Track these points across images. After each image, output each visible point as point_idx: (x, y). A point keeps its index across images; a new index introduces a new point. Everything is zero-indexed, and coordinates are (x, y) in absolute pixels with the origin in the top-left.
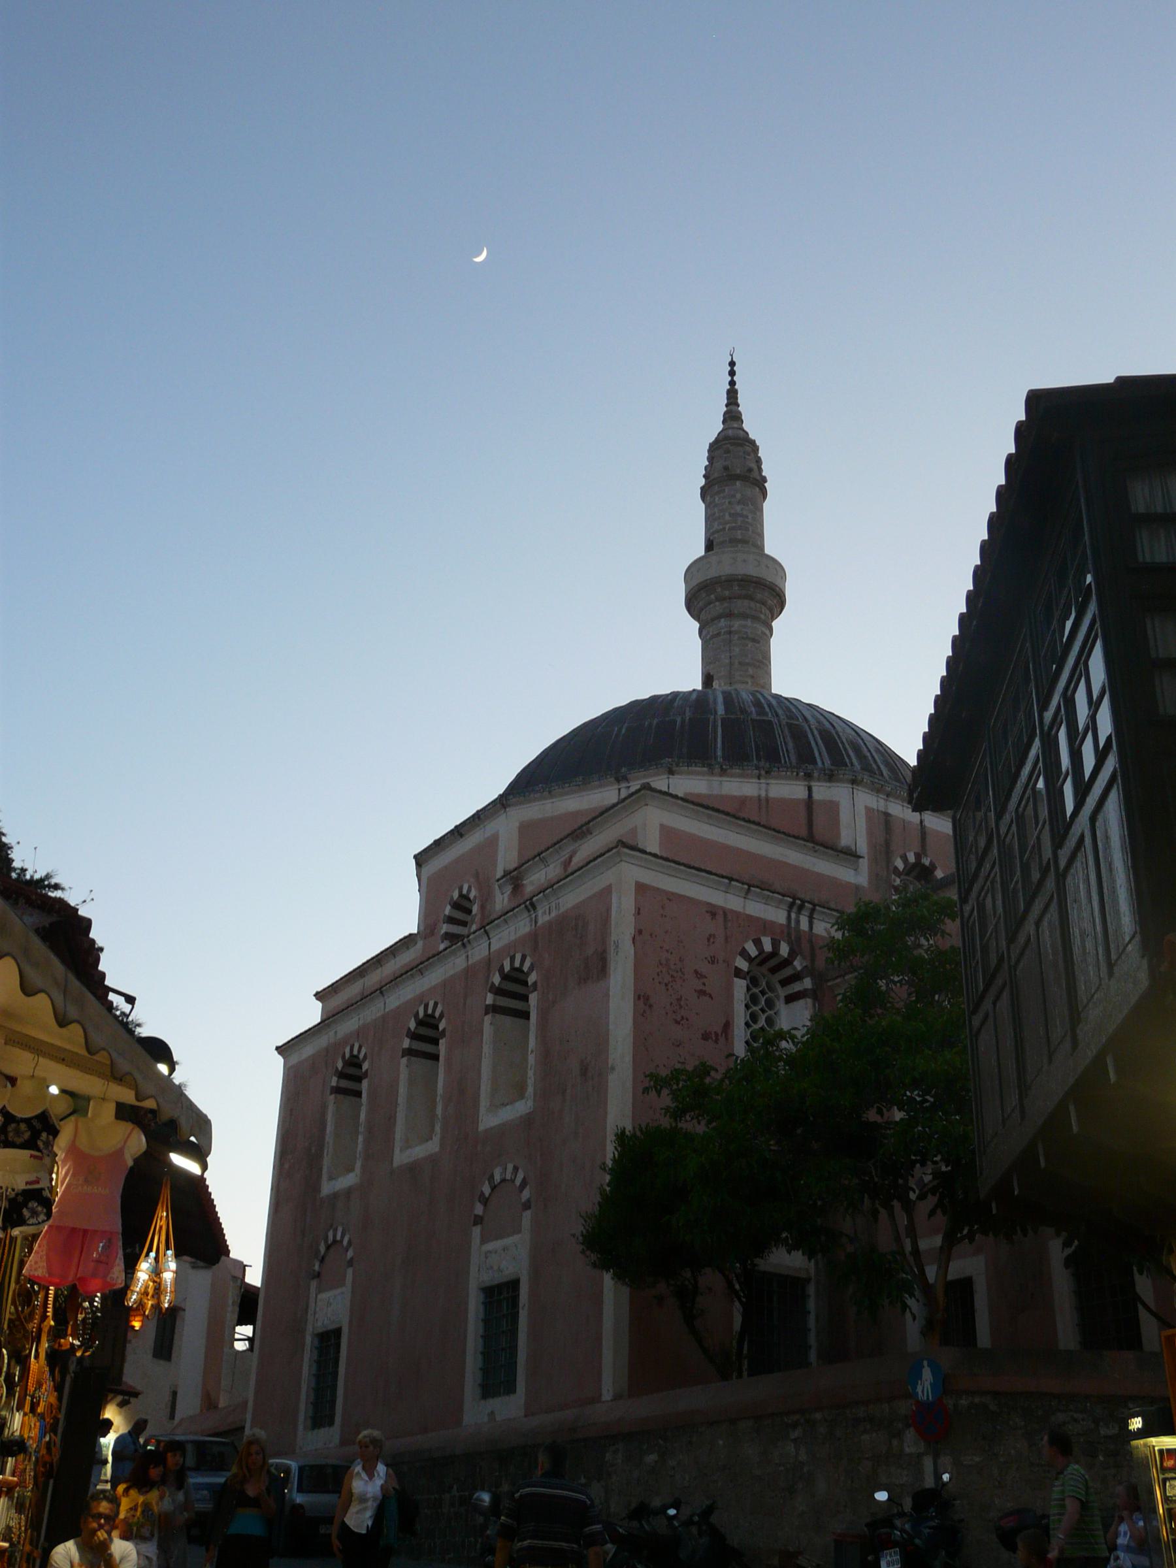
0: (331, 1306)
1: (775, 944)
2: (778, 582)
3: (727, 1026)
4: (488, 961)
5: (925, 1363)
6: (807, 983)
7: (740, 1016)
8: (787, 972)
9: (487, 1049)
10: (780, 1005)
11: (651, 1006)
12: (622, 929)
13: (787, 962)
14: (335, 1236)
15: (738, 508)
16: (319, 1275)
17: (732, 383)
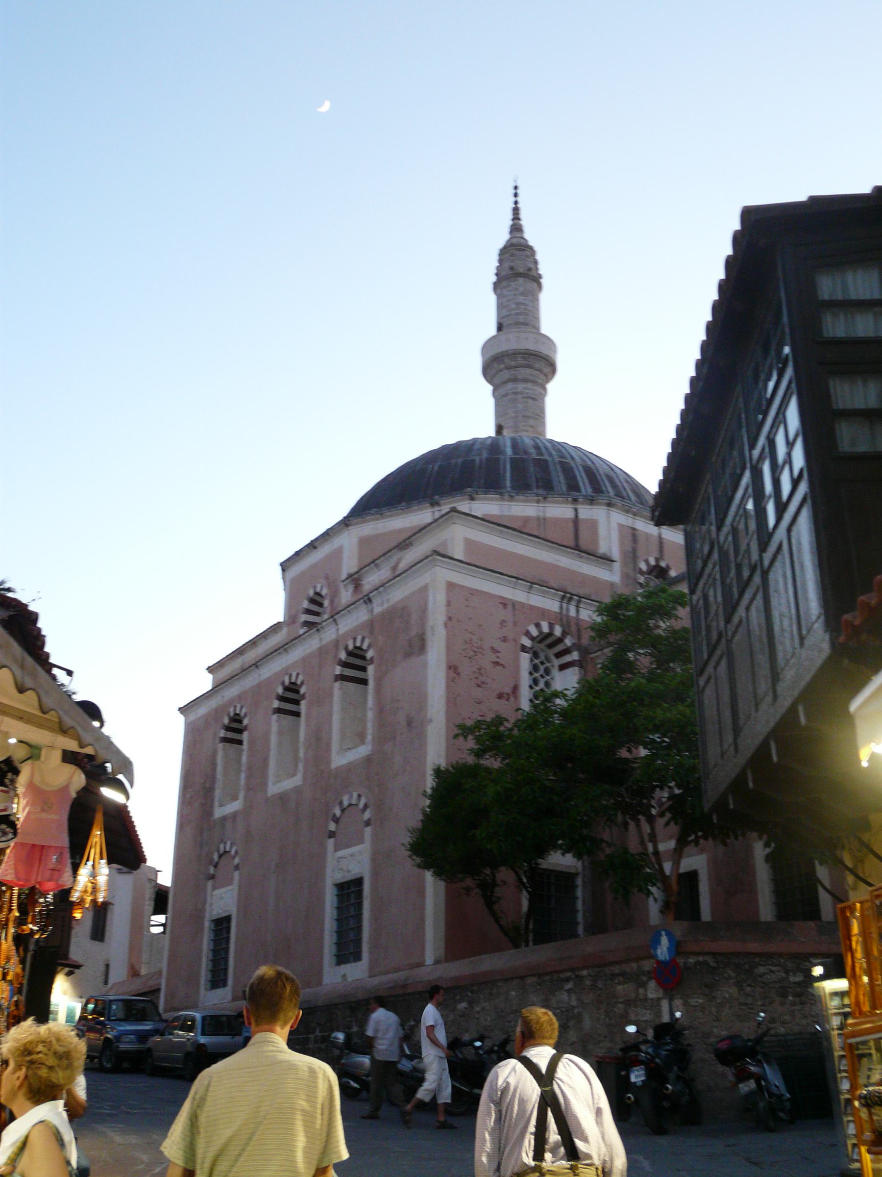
0: (223, 900)
1: (551, 626)
3: (516, 689)
4: (336, 643)
5: (663, 933)
6: (575, 656)
7: (525, 680)
8: (559, 648)
10: (555, 672)
12: (437, 617)
13: (560, 640)
17: (516, 203)
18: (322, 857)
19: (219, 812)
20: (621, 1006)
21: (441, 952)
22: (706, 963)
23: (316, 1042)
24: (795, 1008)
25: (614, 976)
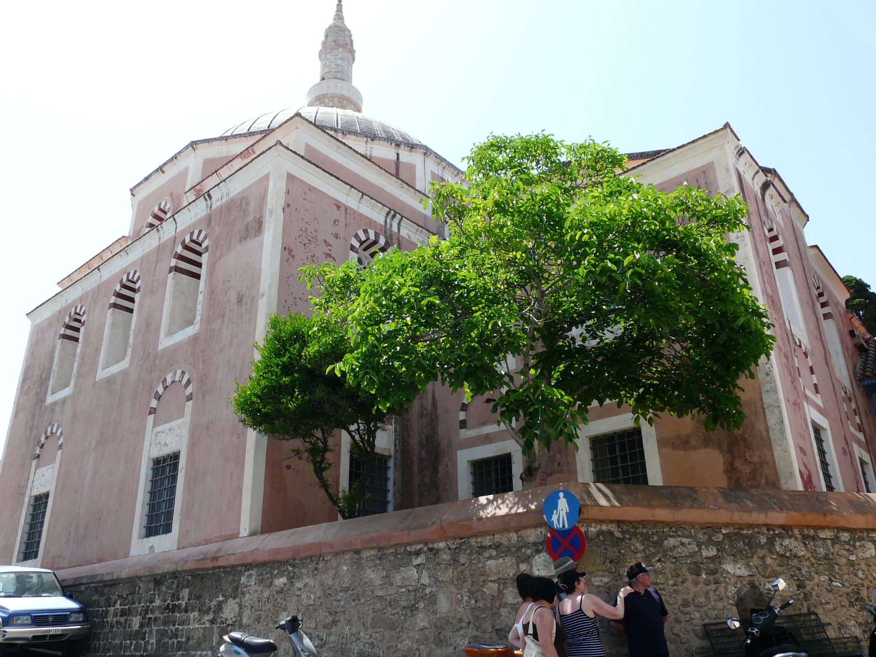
0: (44, 479)
1: (377, 235)
2: (359, 102)
5: (561, 495)
9: (168, 296)
11: (293, 256)
12: (275, 201)
14: (52, 430)
15: (340, 62)
16: (38, 456)
18: (140, 431)
19: (50, 399)
20: (495, 586)
21: (258, 524)
22: (611, 533)
23: (115, 615)
24: (708, 588)
25: (483, 548)
